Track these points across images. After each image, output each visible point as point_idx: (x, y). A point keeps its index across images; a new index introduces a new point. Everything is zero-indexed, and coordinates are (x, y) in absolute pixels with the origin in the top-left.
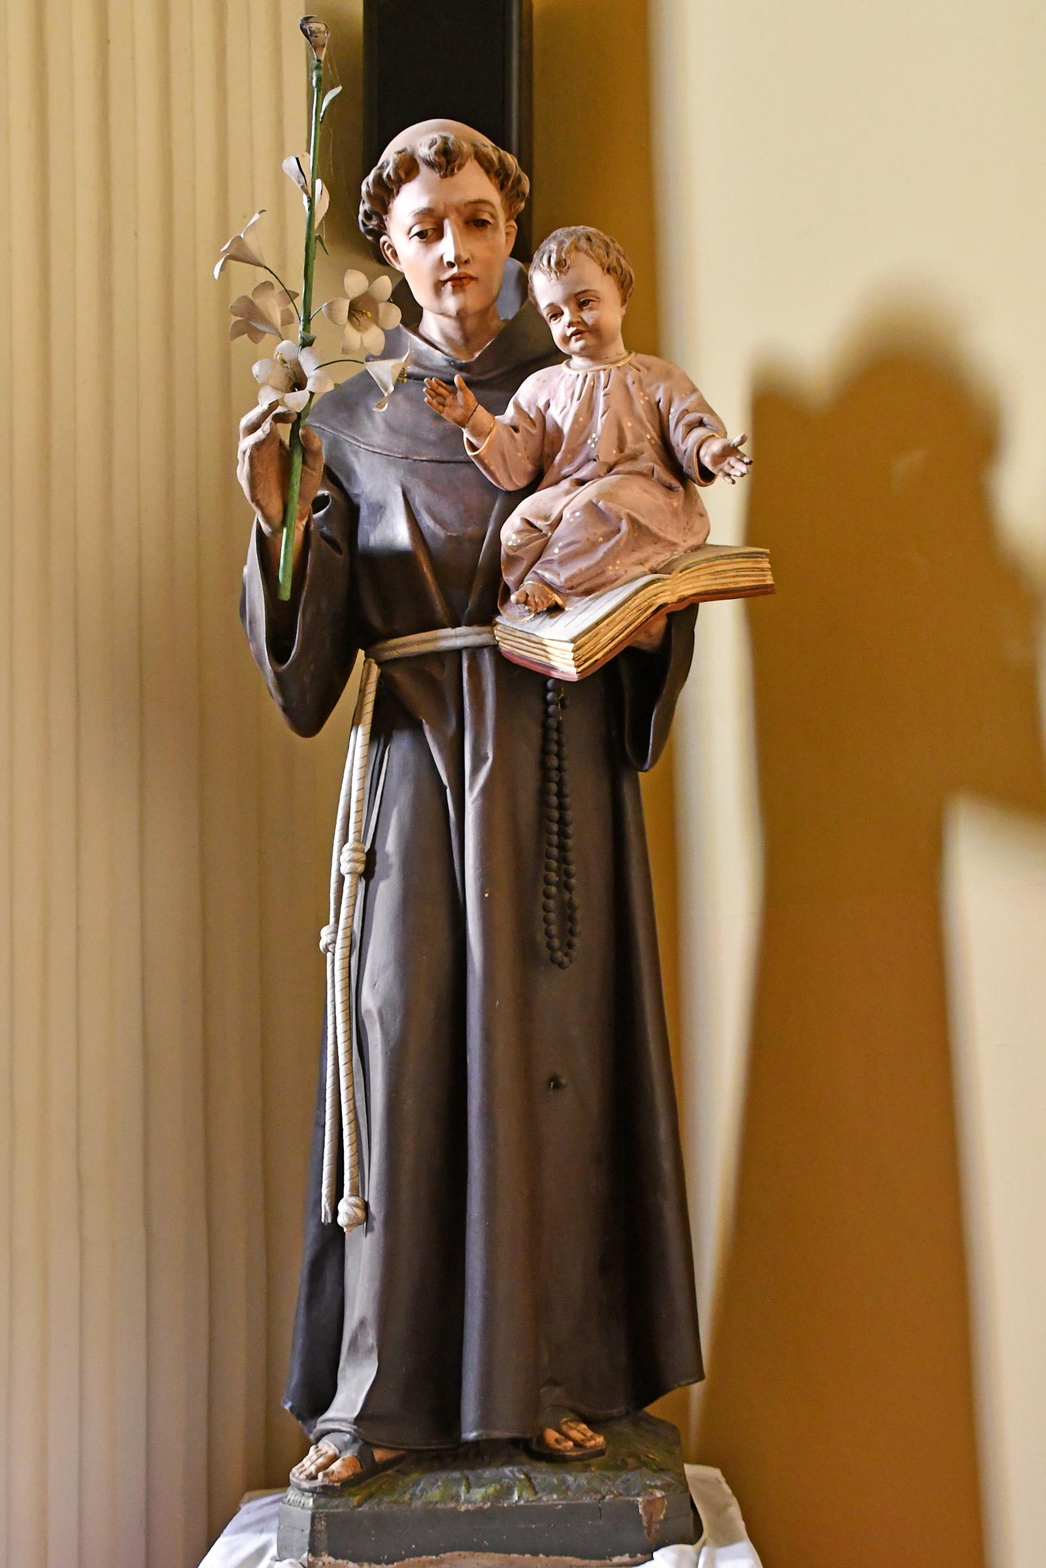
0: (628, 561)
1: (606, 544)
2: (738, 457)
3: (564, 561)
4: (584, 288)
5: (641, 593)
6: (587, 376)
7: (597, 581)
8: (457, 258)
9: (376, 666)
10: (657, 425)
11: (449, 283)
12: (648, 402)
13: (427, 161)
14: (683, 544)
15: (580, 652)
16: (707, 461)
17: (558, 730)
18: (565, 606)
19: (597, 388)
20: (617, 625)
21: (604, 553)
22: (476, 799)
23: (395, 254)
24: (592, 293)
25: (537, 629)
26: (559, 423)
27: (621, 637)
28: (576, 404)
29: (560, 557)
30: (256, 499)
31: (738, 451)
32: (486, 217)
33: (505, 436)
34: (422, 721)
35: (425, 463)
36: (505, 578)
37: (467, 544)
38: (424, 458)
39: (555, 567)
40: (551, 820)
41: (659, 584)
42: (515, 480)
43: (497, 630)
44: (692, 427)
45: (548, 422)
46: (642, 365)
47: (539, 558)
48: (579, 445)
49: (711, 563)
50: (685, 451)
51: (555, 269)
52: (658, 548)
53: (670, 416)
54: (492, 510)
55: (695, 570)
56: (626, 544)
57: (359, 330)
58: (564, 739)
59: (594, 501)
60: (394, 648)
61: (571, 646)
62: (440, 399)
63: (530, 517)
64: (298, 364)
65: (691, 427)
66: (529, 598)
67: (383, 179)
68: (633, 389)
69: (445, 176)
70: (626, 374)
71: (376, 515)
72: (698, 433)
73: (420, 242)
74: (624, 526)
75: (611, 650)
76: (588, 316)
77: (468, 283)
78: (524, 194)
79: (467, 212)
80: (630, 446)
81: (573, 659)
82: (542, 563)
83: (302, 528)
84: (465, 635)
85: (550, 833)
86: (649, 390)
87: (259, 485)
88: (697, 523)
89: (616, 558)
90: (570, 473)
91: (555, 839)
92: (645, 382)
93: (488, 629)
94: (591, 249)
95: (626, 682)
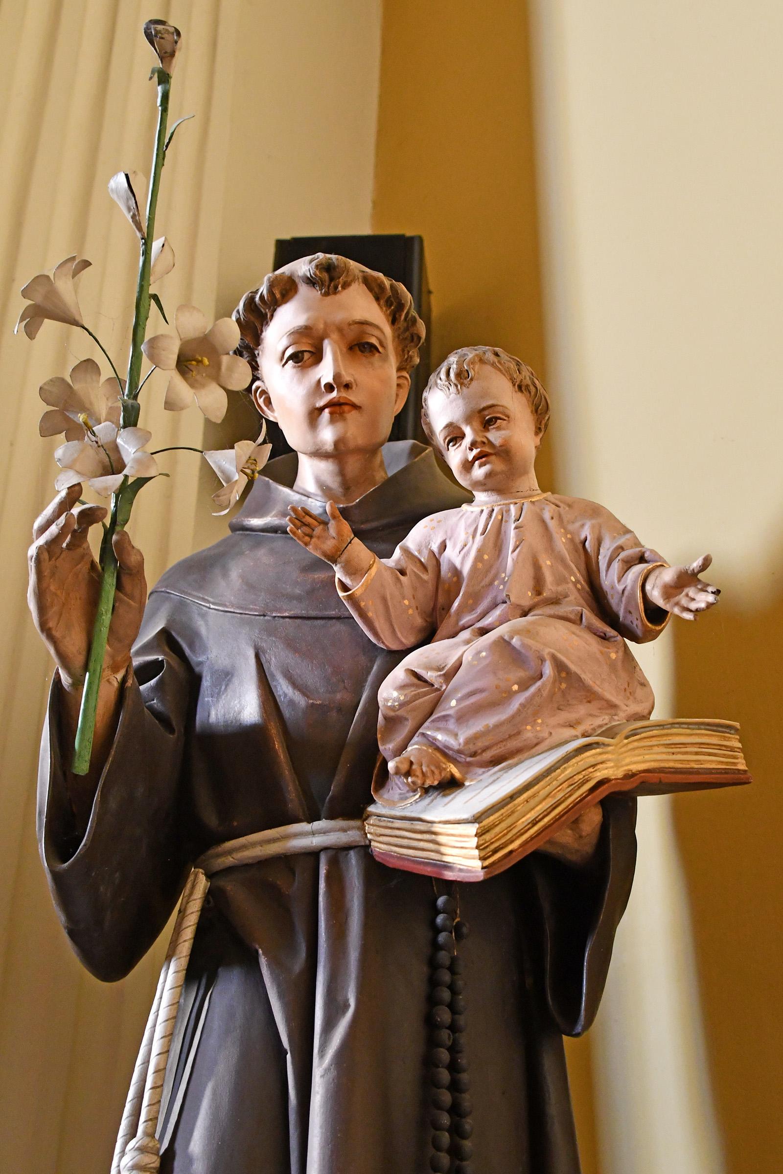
0: (553, 721)
1: (523, 693)
2: (699, 587)
3: (462, 717)
4: (490, 402)
5: (574, 761)
6: (493, 510)
7: (513, 744)
8: (337, 377)
9: (205, 878)
10: (583, 566)
11: (327, 411)
12: (572, 540)
13: (308, 278)
14: (625, 708)
15: (487, 837)
16: (656, 596)
17: (452, 969)
18: (465, 779)
19: (506, 521)
20: (540, 802)
21: (520, 704)
22: (327, 1070)
23: (268, 402)
24: (500, 409)
25: (424, 810)
26: (458, 565)
27: (546, 820)
28: (479, 538)
29: (457, 712)
30: (47, 627)
31: (699, 580)
32: (374, 341)
33: (388, 578)
34: (257, 952)
35: (287, 620)
36: (381, 748)
37: (334, 714)
38: (286, 614)
39: (451, 725)
40: (439, 1108)
41: (598, 750)
42: (399, 635)
43: (368, 824)
44: (629, 566)
45: (444, 568)
46: (561, 502)
47: (431, 714)
48: (483, 587)
49: (666, 731)
50: (623, 591)
51: (455, 382)
52: (592, 708)
53: (600, 557)
54: (369, 673)
55: (645, 738)
56: (552, 695)
57: (192, 386)
58: (460, 983)
59: (506, 638)
60: (230, 852)
61: (473, 829)
62: (307, 530)
63: (419, 667)
64: (116, 448)
65: (628, 564)
66: (414, 767)
67: (255, 303)
68: (552, 524)
69: (327, 294)
70: (542, 509)
71: (221, 685)
72: (638, 569)
73: (295, 367)
74: (548, 670)
75: (532, 838)
76: (495, 436)
77: (349, 412)
78: (419, 338)
79: (352, 334)
80: (550, 587)
81: (477, 848)
82: (433, 721)
83: (116, 684)
84: (324, 832)
85: (437, 1127)
86: (571, 527)
87: (52, 606)
88: (640, 692)
89: (536, 714)
90: (470, 623)
91: (445, 1138)
92: (565, 520)
93: (357, 823)
94: (499, 362)
95: (546, 906)
